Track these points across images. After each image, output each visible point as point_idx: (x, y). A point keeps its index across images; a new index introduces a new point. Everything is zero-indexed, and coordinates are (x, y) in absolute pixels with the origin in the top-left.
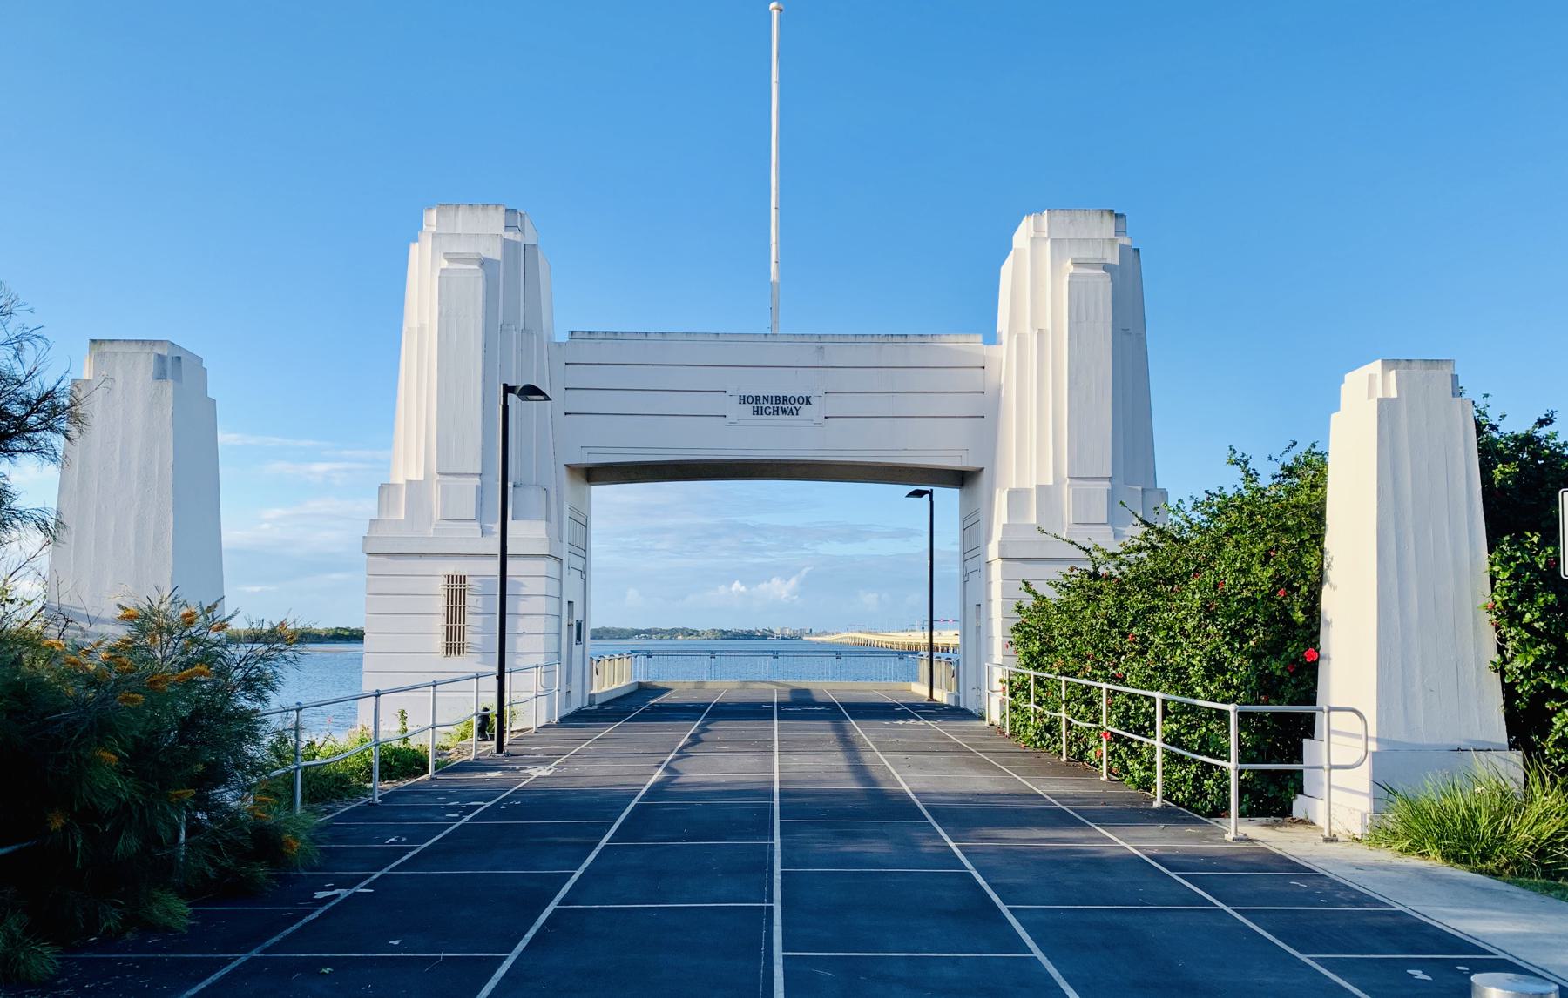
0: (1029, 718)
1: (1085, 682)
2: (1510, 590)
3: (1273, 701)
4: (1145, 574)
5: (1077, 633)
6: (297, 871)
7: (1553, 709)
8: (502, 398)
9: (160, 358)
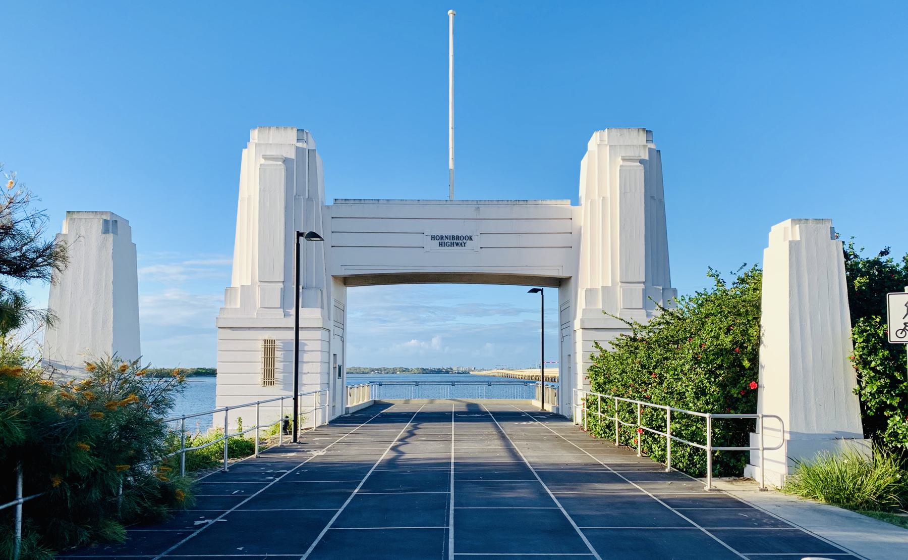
0: (598, 421)
1: (628, 400)
2: (863, 348)
3: (732, 411)
4: (662, 338)
5: (624, 371)
6: (184, 510)
7: (888, 415)
8: (296, 240)
9: (106, 222)
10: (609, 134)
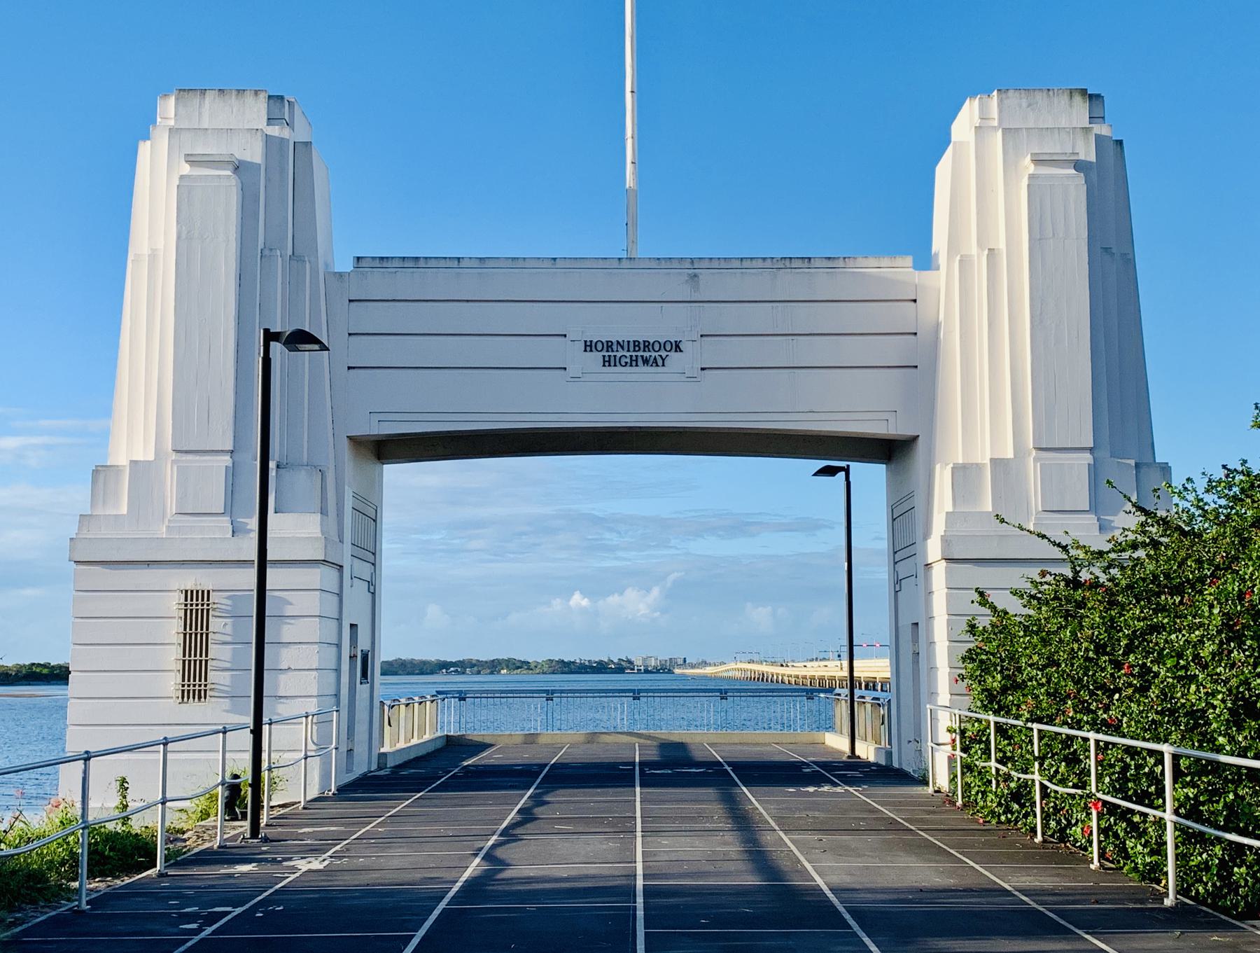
0: (990, 782)
1: (1065, 730)
4: (1144, 580)
10: (1000, 102)
